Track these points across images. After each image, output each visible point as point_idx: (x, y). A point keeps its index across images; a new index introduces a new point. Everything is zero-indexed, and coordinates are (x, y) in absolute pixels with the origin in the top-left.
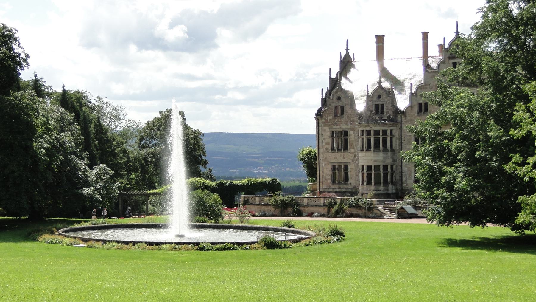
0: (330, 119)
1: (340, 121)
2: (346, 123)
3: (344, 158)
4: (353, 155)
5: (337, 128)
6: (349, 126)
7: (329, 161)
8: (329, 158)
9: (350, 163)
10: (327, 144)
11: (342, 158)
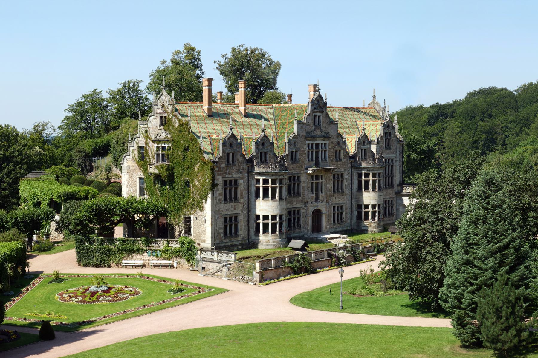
0: (223, 167)
2: (237, 172)
3: (235, 209)
5: (229, 177)
6: (239, 175)
10: (220, 195)
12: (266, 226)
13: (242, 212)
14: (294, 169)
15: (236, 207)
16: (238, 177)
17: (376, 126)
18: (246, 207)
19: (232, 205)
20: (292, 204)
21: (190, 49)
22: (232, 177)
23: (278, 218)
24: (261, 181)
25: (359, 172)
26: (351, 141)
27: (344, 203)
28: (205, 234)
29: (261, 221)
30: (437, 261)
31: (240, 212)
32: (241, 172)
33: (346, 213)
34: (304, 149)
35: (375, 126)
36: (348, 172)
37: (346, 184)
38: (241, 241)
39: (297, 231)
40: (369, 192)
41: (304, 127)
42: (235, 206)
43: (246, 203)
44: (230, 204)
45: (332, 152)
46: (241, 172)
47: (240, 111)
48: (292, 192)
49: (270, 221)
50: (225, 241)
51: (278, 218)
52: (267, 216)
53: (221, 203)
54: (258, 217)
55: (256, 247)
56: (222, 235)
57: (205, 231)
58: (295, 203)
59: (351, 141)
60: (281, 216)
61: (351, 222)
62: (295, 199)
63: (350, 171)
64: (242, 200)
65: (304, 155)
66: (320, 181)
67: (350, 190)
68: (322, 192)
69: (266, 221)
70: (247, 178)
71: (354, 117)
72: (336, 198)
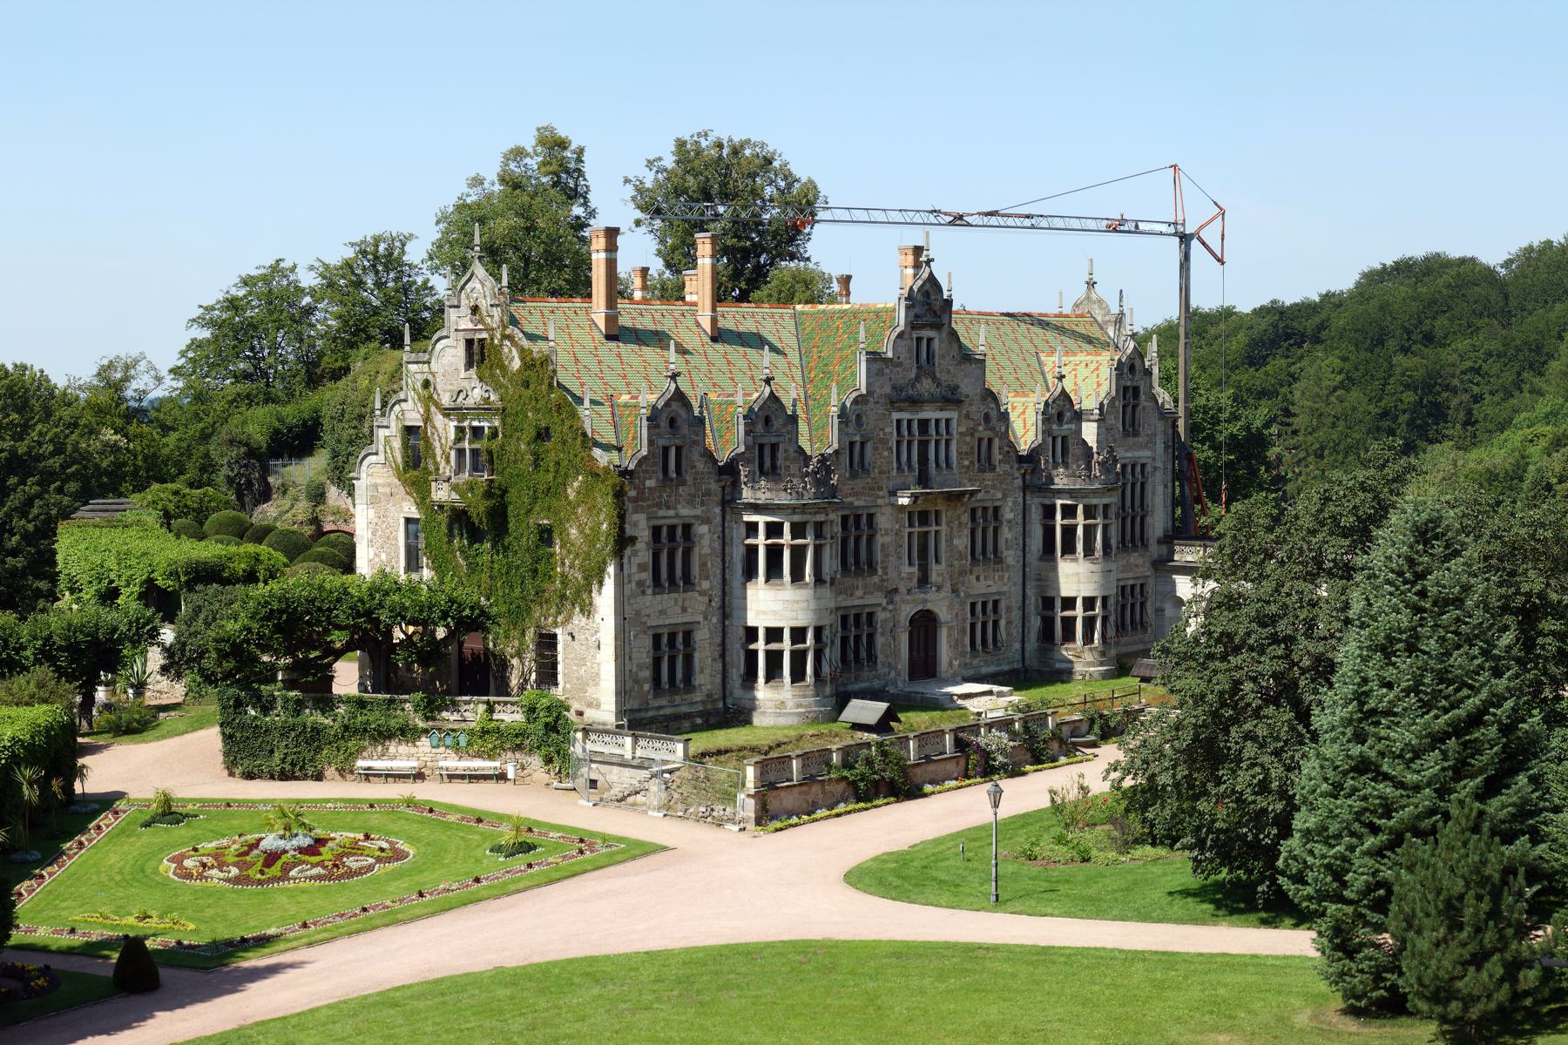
2: (691, 503)
3: (684, 610)
5: (667, 516)
6: (698, 512)
7: (645, 623)
8: (647, 612)
10: (642, 568)
13: (705, 618)
16: (695, 517)
17: (1097, 369)
18: (716, 603)
19: (676, 600)
20: (852, 595)
21: (554, 144)
22: (677, 516)
23: (810, 635)
24: (761, 529)
25: (1047, 502)
26: (1024, 413)
28: (597, 684)
32: (702, 502)
34: (885, 434)
35: (1092, 367)
36: (1015, 502)
40: (1076, 560)
42: (684, 600)
43: (717, 592)
45: (968, 444)
46: (703, 503)
47: (698, 325)
48: (851, 560)
49: (786, 645)
51: (810, 635)
52: (779, 631)
53: (643, 593)
57: (598, 675)
58: (859, 593)
59: (1024, 413)
60: (818, 631)
62: (860, 582)
63: (1020, 500)
65: (886, 454)
68: (937, 561)
70: (718, 519)
71: (1031, 341)
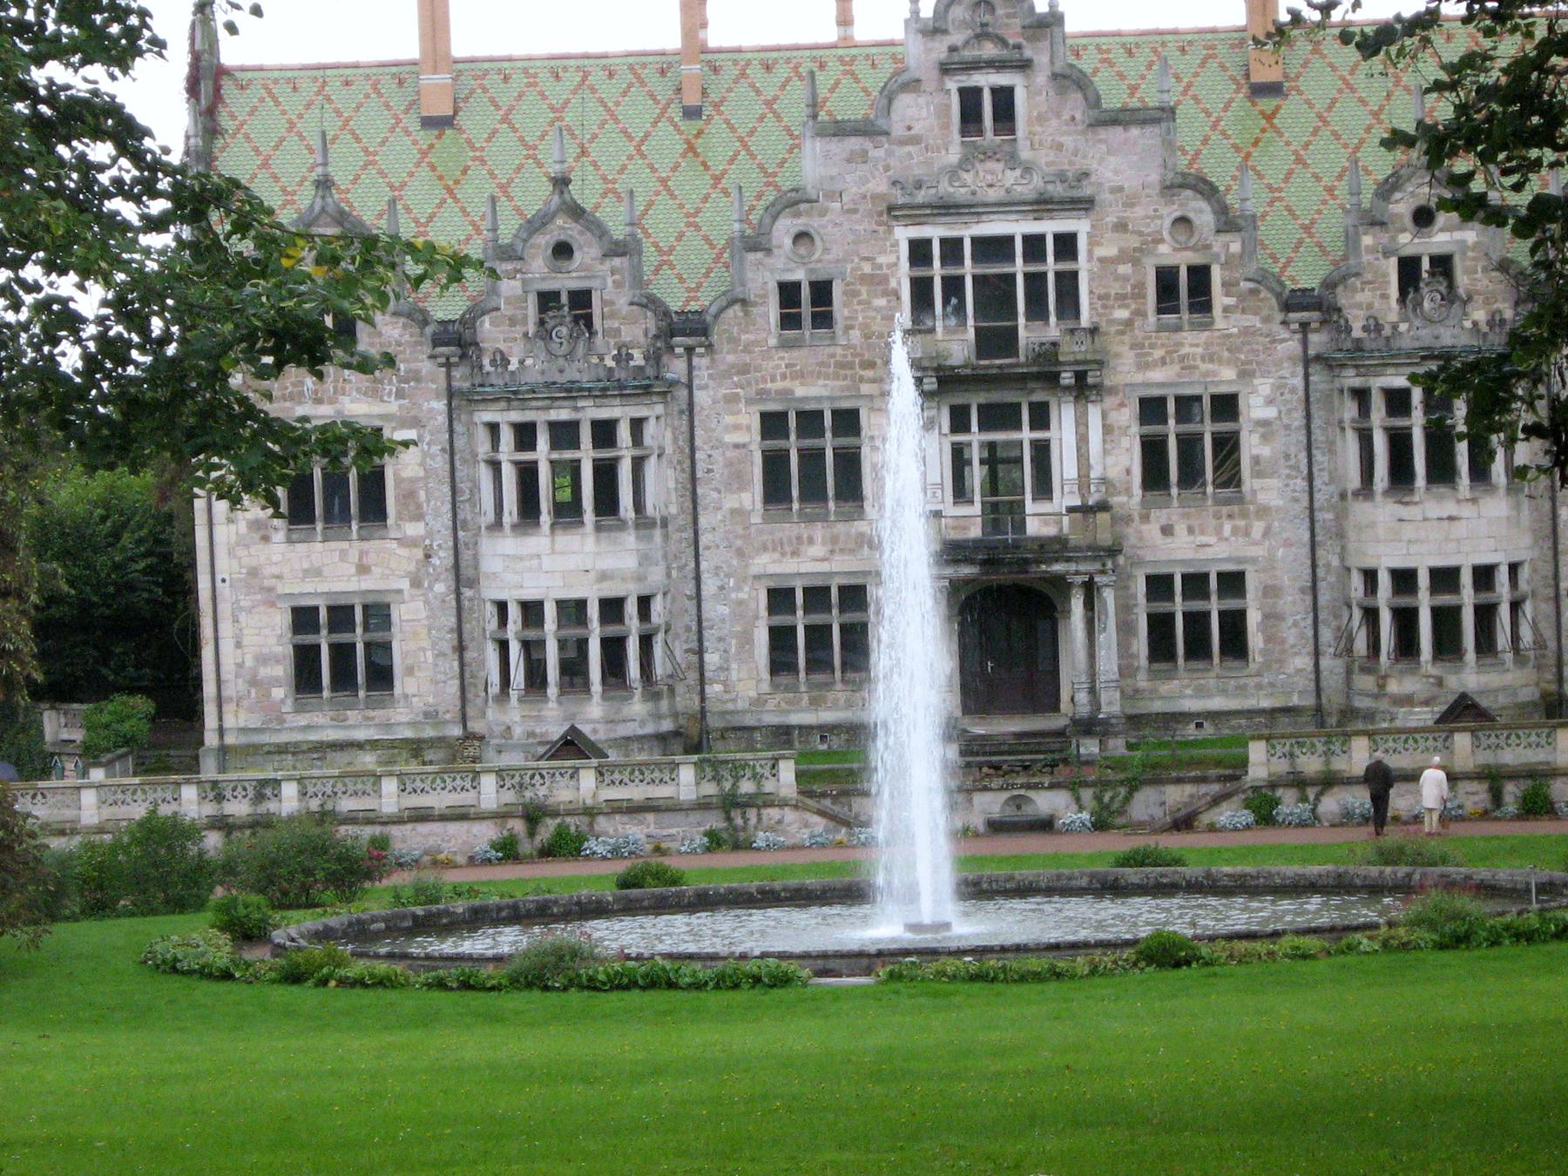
1: (336, 381)
3: (363, 569)
4: (419, 553)
6: (393, 407)
8: (275, 570)
9: (400, 591)
11: (353, 570)
12: (1446, 620)
14: (801, 376)
15: (371, 559)
18: (443, 558)
27: (1254, 560)
29: (1425, 603)
30: (572, 932)
31: (405, 584)
33: (1271, 617)
37: (1265, 451)
38: (413, 724)
39: (839, 693)
41: (873, 153)
42: (362, 554)
43: (443, 540)
44: (333, 545)
45: (1125, 279)
46: (400, 394)
49: (1467, 597)
50: (303, 720)
52: (581, 604)
54: (1370, 576)
55: (198, 772)
56: (278, 693)
58: (817, 550)
61: (1317, 665)
62: (819, 531)
63: (1298, 382)
64: (414, 529)
65: (881, 302)
66: (1026, 435)
67: (1301, 484)
69: (1446, 599)
72: (1167, 531)
